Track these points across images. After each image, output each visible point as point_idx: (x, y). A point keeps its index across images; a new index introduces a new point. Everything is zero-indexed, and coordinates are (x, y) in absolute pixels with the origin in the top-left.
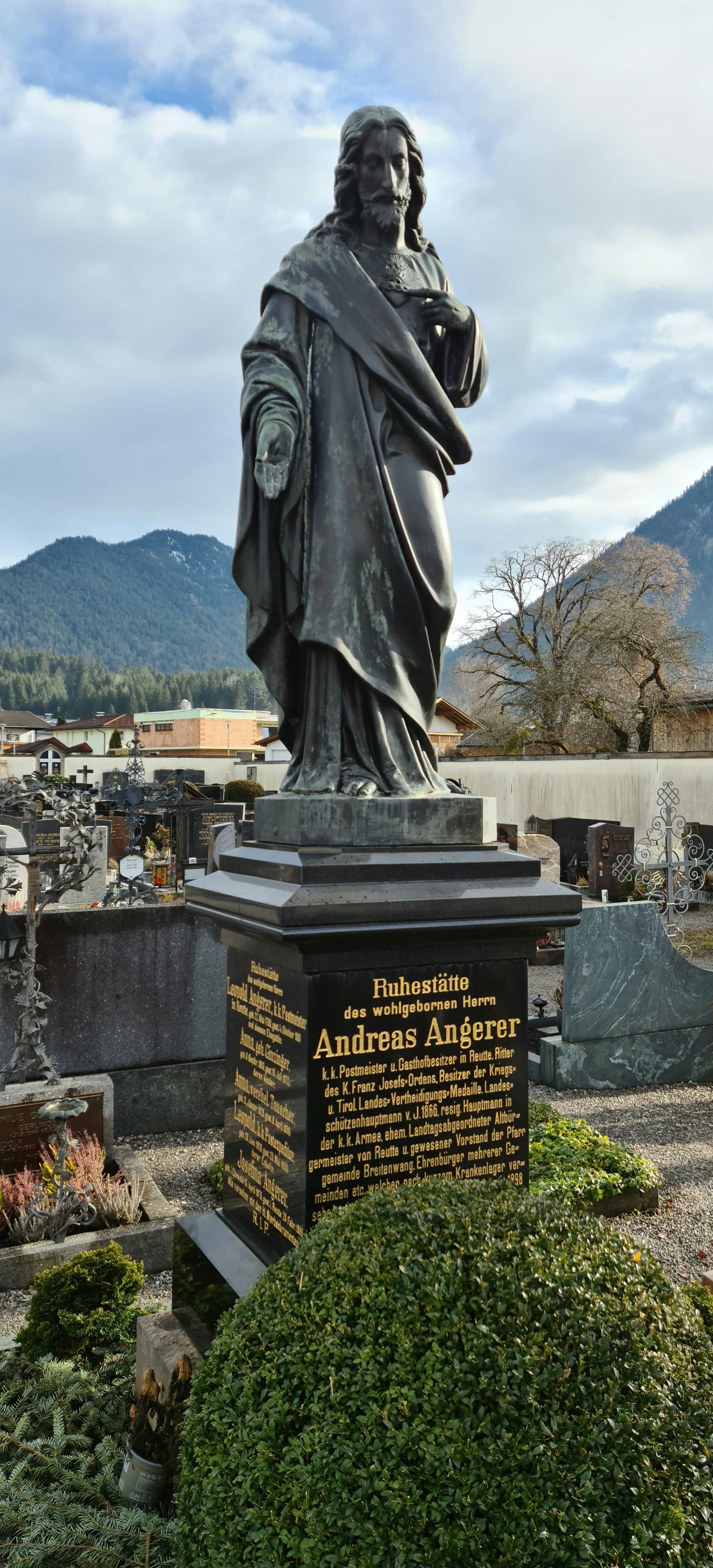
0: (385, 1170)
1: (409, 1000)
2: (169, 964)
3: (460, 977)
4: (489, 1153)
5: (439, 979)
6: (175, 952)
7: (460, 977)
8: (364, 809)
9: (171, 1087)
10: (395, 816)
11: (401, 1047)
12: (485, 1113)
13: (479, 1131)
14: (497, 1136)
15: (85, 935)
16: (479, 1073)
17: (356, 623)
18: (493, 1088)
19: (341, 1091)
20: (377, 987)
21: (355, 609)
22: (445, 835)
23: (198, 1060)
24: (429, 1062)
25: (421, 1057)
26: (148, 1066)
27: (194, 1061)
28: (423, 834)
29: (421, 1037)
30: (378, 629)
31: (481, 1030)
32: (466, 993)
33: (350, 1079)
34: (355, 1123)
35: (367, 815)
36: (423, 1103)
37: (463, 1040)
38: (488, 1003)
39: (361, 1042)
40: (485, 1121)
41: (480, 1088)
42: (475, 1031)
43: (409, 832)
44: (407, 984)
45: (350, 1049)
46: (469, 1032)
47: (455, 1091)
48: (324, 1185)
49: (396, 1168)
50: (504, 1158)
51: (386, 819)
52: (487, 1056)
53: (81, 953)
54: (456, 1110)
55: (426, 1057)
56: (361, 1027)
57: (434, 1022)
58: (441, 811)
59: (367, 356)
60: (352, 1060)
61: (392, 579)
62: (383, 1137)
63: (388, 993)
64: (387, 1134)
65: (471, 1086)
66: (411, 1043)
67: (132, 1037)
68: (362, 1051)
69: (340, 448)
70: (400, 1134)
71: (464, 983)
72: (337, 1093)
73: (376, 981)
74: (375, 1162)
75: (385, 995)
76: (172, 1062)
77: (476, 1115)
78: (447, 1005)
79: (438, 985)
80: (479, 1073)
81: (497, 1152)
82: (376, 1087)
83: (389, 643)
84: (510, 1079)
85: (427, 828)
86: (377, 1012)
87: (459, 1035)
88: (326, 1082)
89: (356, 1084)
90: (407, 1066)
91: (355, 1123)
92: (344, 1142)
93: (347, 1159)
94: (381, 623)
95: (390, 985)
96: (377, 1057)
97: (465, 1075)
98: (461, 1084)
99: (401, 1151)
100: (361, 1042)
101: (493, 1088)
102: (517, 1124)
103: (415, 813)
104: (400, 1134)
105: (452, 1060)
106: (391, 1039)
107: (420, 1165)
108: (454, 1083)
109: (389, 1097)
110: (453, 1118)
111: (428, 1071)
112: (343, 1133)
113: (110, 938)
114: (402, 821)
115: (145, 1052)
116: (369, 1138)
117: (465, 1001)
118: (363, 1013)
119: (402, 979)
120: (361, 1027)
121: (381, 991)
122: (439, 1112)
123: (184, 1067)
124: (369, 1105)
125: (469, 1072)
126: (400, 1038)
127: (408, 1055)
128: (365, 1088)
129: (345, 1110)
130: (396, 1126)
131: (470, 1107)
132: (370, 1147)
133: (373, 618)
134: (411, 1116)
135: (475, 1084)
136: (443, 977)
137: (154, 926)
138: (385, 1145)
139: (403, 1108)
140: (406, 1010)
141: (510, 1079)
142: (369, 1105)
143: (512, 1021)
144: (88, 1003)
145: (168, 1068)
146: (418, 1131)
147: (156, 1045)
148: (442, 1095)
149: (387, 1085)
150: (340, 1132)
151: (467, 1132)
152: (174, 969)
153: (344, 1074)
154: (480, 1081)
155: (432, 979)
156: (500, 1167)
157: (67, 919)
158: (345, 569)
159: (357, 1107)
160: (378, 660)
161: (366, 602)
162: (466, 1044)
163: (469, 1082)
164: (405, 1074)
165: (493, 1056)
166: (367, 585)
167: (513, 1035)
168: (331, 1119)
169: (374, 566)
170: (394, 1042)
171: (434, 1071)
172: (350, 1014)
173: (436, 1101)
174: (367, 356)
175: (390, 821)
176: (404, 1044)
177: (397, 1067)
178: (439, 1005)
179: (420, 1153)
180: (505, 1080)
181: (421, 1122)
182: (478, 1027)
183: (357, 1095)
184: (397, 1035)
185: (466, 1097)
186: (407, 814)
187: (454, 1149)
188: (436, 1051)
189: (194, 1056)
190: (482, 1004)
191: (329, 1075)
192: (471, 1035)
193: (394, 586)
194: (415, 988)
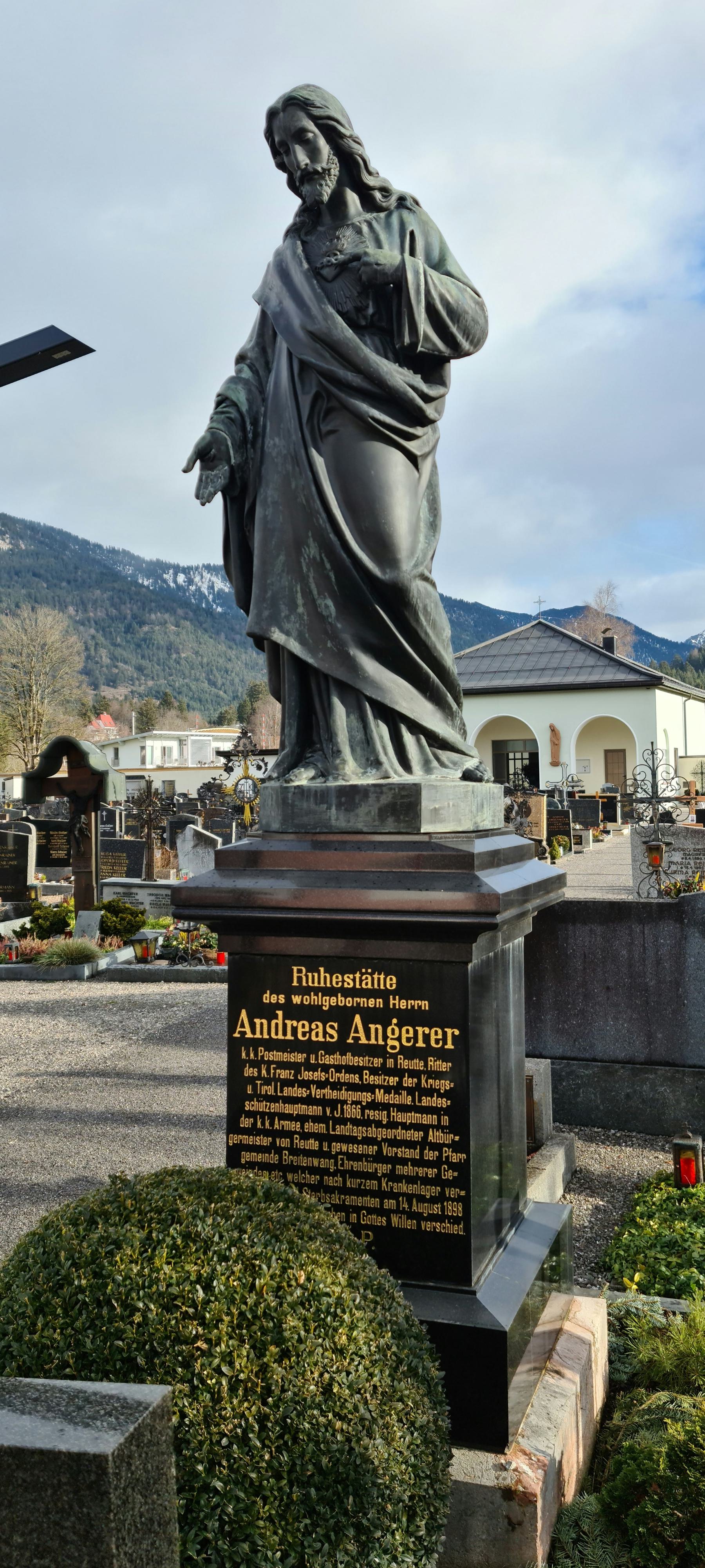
0: (304, 1162)
1: (330, 992)
2: (659, 962)
3: (386, 976)
4: (421, 1171)
5: (362, 974)
6: (664, 951)
7: (386, 976)
8: (290, 795)
9: (664, 1089)
10: (322, 802)
11: (321, 1039)
12: (417, 1127)
13: (410, 1144)
14: (430, 1155)
15: (574, 924)
16: (408, 1082)
17: (301, 610)
18: (426, 1101)
19: (260, 1072)
20: (295, 975)
21: (299, 595)
22: (377, 823)
23: (694, 1066)
24: (349, 1059)
25: (343, 1054)
26: (641, 1064)
27: (690, 1067)
28: (352, 821)
29: (344, 1032)
30: (324, 613)
31: (411, 1035)
32: (394, 993)
33: (269, 1063)
34: (275, 1107)
35: (293, 801)
36: (344, 1102)
37: (390, 1043)
38: (420, 1007)
39: (278, 1028)
40: (417, 1136)
41: (410, 1098)
42: (404, 1036)
43: (337, 819)
44: (328, 975)
45: (269, 1033)
46: (397, 1036)
47: (380, 1095)
48: (243, 1161)
49: (316, 1162)
50: (437, 1181)
51: (313, 806)
52: (417, 1064)
53: (571, 941)
54: (383, 1116)
55: (349, 1054)
56: (280, 1013)
57: (357, 1019)
58: (372, 798)
59: (353, 338)
60: (271, 1045)
61: (330, 561)
62: (302, 1127)
63: (307, 982)
64: (306, 1126)
65: (400, 1094)
66: (332, 1037)
67: (624, 1031)
68: (280, 1036)
69: (277, 440)
70: (321, 1128)
71: (391, 982)
72: (256, 1074)
73: (295, 968)
74: (294, 1151)
75: (304, 984)
76: (667, 1064)
77: (405, 1127)
78: (371, 1003)
79: (361, 981)
80: (408, 1082)
81: (432, 1172)
82: (295, 1075)
83: (339, 626)
84: (447, 1095)
85: (357, 816)
86: (296, 999)
87: (385, 1037)
88: (245, 1061)
89: (275, 1069)
90: (329, 1060)
91: (275, 1107)
92: (263, 1124)
93: (266, 1141)
94: (327, 607)
95: (310, 975)
96: (294, 1046)
97: (393, 1081)
98: (388, 1089)
99: (321, 1146)
100: (278, 1028)
101: (426, 1101)
102: (455, 1147)
103: (343, 799)
104: (321, 1128)
105: (377, 1062)
106: (311, 1030)
107: (342, 1165)
108: (380, 1087)
109: (374, 1093)
110: (379, 1124)
111: (350, 1069)
112: (263, 1115)
113: (599, 929)
114: (329, 808)
115: (638, 1049)
116: (288, 1125)
117: (392, 1002)
118: (282, 999)
119: (322, 969)
120: (280, 1013)
121: (300, 979)
122: (363, 1114)
123: (678, 1071)
124: (287, 1091)
125: (397, 1079)
126: (320, 1030)
127: (329, 1048)
128: (284, 1074)
129: (263, 1093)
130: (316, 1119)
131: (400, 1117)
132: (289, 1134)
133: (319, 602)
134: (332, 1112)
135: (404, 1093)
136: (367, 973)
137: (641, 921)
138: (305, 1136)
139: (323, 1102)
140: (328, 1002)
141: (447, 1095)
142: (287, 1091)
143: (449, 1031)
144: (581, 990)
145: (662, 1070)
146: (340, 1130)
147: (650, 1044)
148: (366, 1097)
149: (306, 1075)
150: (258, 1112)
151: (394, 1143)
152: (664, 968)
153: (263, 1057)
154: (410, 1091)
155: (355, 973)
156: (434, 1190)
157: (557, 907)
158: (282, 558)
159: (276, 1091)
160: (329, 645)
161: (309, 588)
162: (393, 1047)
163: (398, 1088)
164: (325, 1068)
165: (426, 1065)
166: (309, 570)
167: (449, 1046)
168: (250, 1098)
169: (312, 550)
170: (313, 1033)
171: (358, 1070)
172: (269, 998)
173: (359, 1103)
174: (353, 338)
175: (317, 808)
176: (324, 1037)
177: (317, 1059)
178: (362, 1001)
179: (341, 1153)
180: (440, 1095)
181: (343, 1121)
182: (408, 1032)
183: (276, 1080)
184: (317, 1027)
185: (394, 1105)
186: (334, 801)
187: (378, 1157)
188: (358, 1049)
189: (690, 1062)
190: (413, 1007)
191: (248, 1055)
192: (399, 1039)
193: (333, 567)
194: (336, 980)
